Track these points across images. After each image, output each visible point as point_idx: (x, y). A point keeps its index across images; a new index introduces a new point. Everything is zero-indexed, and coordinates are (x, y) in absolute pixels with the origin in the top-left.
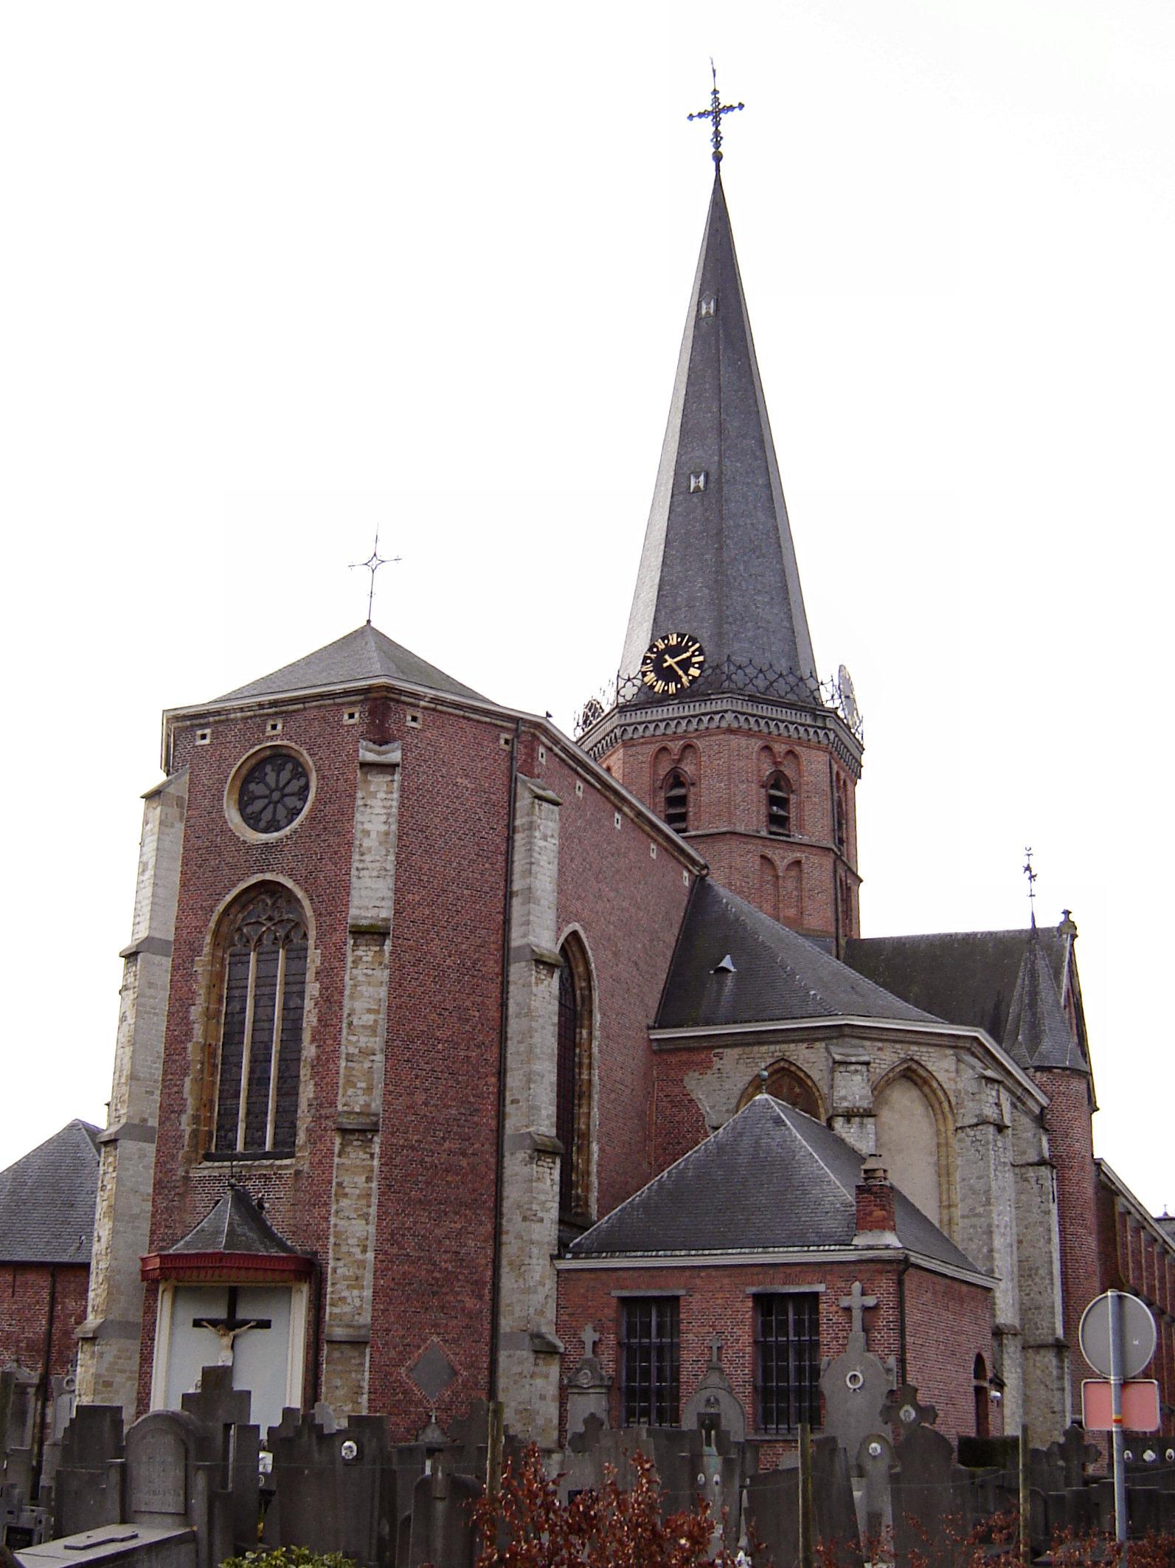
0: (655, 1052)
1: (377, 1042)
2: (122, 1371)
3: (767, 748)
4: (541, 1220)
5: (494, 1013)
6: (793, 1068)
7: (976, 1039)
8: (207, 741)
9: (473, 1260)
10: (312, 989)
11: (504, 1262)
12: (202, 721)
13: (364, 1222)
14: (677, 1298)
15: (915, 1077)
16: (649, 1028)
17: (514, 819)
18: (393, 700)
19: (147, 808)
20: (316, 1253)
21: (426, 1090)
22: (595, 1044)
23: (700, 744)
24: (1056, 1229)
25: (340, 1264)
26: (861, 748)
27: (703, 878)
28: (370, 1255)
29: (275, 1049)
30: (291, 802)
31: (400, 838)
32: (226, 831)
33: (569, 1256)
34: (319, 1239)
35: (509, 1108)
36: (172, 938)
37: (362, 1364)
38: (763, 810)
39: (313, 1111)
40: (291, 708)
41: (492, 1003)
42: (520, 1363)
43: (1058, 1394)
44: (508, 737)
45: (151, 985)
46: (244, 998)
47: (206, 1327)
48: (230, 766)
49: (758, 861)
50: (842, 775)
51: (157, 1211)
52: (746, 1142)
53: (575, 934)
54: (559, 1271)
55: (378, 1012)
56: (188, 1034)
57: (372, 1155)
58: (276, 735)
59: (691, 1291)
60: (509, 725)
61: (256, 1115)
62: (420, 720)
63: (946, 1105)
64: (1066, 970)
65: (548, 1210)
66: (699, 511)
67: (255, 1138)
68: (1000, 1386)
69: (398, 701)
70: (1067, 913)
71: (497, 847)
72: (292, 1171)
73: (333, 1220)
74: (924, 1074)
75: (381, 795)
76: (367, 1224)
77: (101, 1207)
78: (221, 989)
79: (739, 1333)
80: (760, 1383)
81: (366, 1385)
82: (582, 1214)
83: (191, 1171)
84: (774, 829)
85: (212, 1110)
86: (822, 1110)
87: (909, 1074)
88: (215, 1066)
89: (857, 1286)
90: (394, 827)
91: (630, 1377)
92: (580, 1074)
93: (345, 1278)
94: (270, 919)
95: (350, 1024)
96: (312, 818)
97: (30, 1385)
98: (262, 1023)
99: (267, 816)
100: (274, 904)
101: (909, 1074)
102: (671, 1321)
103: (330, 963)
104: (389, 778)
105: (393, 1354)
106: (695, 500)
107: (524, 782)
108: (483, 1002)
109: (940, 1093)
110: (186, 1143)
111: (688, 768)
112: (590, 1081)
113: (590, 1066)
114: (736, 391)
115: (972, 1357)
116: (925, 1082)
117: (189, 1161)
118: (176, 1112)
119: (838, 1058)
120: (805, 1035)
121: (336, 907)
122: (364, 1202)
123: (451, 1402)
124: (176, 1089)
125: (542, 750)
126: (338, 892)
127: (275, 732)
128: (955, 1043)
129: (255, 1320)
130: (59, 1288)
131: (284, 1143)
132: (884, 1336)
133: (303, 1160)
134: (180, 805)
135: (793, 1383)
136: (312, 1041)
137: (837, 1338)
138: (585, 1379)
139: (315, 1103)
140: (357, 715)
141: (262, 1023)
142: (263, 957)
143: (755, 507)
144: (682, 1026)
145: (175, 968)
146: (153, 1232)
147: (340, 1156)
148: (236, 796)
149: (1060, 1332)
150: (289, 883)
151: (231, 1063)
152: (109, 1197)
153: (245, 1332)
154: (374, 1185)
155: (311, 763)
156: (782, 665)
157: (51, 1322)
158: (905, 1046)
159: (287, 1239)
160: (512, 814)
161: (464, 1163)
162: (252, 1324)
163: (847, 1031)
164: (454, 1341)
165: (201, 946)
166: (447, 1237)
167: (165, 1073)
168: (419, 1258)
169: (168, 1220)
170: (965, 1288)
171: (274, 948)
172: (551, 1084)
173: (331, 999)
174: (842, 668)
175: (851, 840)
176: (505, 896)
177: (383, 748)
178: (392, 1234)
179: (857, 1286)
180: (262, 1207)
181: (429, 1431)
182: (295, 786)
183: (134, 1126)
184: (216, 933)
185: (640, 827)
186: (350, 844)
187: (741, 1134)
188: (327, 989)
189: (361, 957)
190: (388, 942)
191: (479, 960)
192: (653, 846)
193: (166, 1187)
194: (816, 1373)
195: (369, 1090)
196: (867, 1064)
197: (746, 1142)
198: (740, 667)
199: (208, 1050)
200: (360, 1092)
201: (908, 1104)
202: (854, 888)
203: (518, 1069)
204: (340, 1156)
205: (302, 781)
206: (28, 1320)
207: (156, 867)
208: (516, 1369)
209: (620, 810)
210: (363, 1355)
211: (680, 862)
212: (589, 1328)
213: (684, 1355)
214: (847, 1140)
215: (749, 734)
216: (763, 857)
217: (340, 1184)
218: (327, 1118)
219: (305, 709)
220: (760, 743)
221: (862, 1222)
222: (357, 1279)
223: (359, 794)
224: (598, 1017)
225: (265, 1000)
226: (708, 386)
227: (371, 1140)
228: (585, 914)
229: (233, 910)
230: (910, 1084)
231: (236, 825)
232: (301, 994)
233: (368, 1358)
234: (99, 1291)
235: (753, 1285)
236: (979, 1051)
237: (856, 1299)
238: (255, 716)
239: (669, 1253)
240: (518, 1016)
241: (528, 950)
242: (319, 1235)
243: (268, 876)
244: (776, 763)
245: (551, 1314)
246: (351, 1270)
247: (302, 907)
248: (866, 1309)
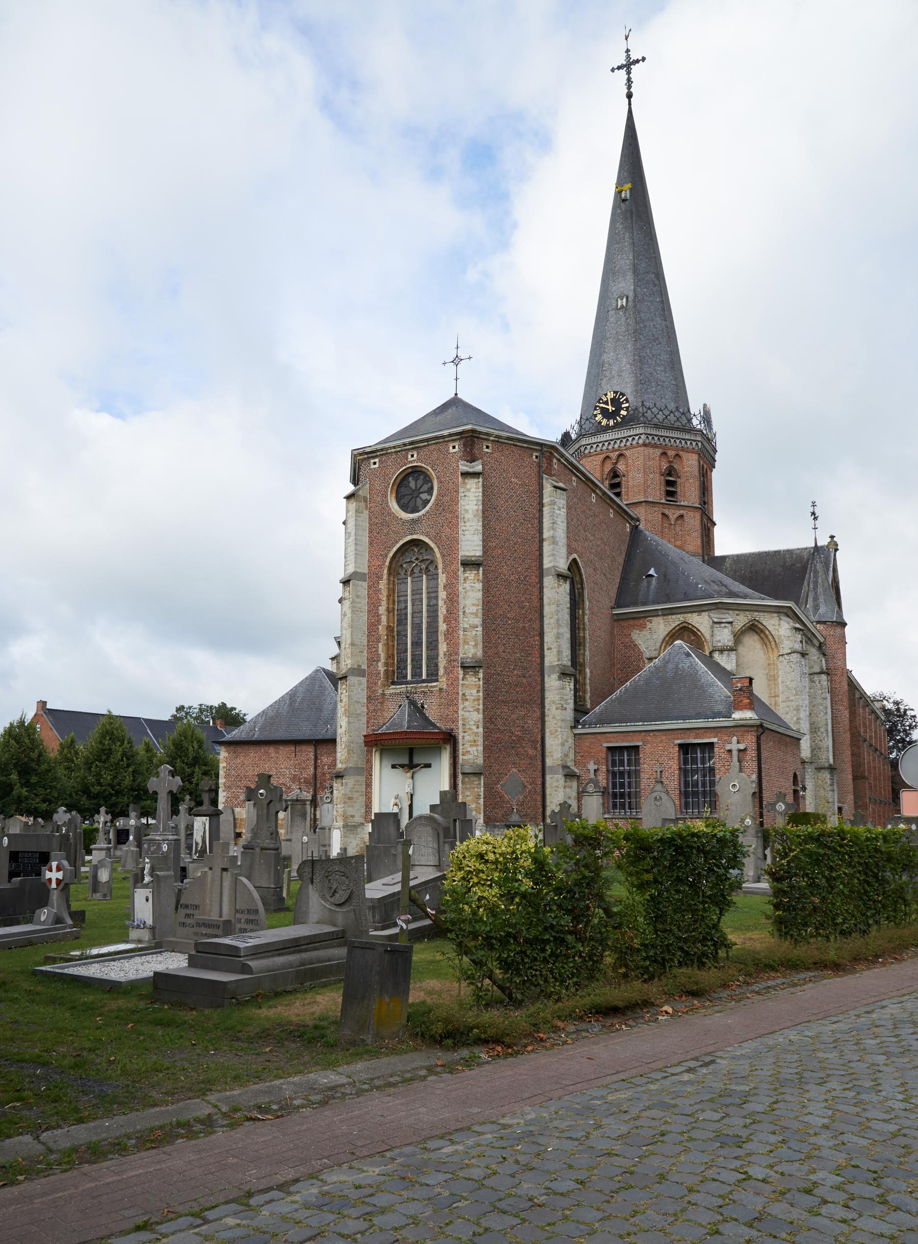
0: (615, 620)
1: (478, 621)
3: (664, 454)
4: (566, 709)
5: (536, 603)
6: (690, 627)
7: (790, 607)
8: (377, 466)
9: (531, 730)
10: (442, 595)
11: (547, 730)
12: (373, 455)
14: (638, 747)
15: (757, 630)
16: (612, 608)
17: (542, 499)
18: (476, 437)
19: (347, 504)
20: (452, 729)
21: (504, 645)
22: (586, 617)
23: (627, 453)
24: (829, 707)
25: (466, 734)
26: (715, 451)
27: (637, 527)
28: (481, 730)
29: (424, 626)
30: (424, 496)
31: (483, 513)
32: (390, 513)
33: (580, 727)
35: (546, 652)
36: (366, 571)
37: (480, 784)
38: (663, 488)
40: (421, 445)
41: (535, 599)
42: (557, 781)
43: (831, 793)
44: (537, 454)
45: (358, 596)
46: (406, 602)
48: (390, 479)
49: (660, 515)
50: (705, 466)
52: (671, 666)
53: (574, 560)
54: (575, 735)
55: (478, 605)
56: (379, 621)
57: (479, 679)
58: (413, 459)
59: (645, 742)
60: (538, 448)
61: (417, 660)
62: (490, 448)
63: (773, 643)
64: (831, 569)
65: (568, 704)
66: (623, 319)
67: (417, 672)
68: (804, 789)
69: (478, 438)
70: (832, 537)
71: (534, 515)
73: (461, 713)
74: (762, 627)
75: (473, 490)
77: (340, 710)
78: (394, 597)
79: (671, 763)
80: (683, 789)
81: (482, 794)
82: (582, 705)
84: (668, 499)
85: (393, 660)
86: (706, 648)
87: (753, 628)
88: (393, 637)
89: (735, 739)
90: (481, 507)
91: (614, 786)
92: (579, 633)
93: (469, 741)
94: (417, 559)
95: (464, 612)
96: (436, 504)
97: (308, 800)
98: (417, 613)
99: (411, 505)
100: (419, 551)
101: (753, 628)
102: (635, 759)
103: (451, 581)
104: (477, 480)
105: (494, 778)
106: (621, 313)
107: (547, 479)
108: (530, 598)
109: (770, 637)
111: (621, 467)
112: (584, 637)
113: (584, 629)
114: (643, 245)
115: (792, 775)
116: (762, 631)
117: (384, 685)
119: (716, 620)
120: (669, 611)
121: (452, 551)
123: (524, 801)
125: (555, 461)
126: (451, 544)
127: (413, 459)
128: (779, 610)
130: (318, 752)
131: (432, 675)
132: (751, 763)
133: (443, 682)
134: (365, 501)
135: (700, 789)
136: (444, 621)
137: (724, 766)
138: (591, 788)
140: (457, 447)
141: (417, 613)
142: (414, 580)
143: (655, 315)
144: (629, 606)
145: (369, 587)
146: (368, 722)
147: (463, 680)
148: (394, 495)
149: (831, 761)
150: (427, 540)
151: (402, 635)
152: (345, 705)
153: (419, 770)
154: (481, 694)
155: (434, 474)
156: (672, 406)
157: (316, 768)
158: (752, 613)
160: (541, 497)
161: (524, 681)
163: (720, 606)
164: (524, 771)
165: (382, 575)
166: (518, 719)
167: (368, 641)
168: (505, 730)
170: (788, 739)
171: (420, 575)
172: (568, 639)
173: (453, 600)
174: (705, 406)
175: (710, 503)
176: (539, 541)
177: (473, 464)
178: (490, 719)
179: (735, 739)
180: (423, 707)
181: (513, 816)
182: (425, 488)
183: (355, 669)
184: (390, 568)
185: (605, 501)
186: (457, 517)
187: (668, 662)
188: (450, 594)
189: (468, 577)
190: (481, 569)
191: (527, 576)
192: (611, 511)
194: (713, 783)
195: (476, 645)
196: (731, 623)
197: (671, 666)
198: (649, 409)
199: (389, 629)
201: (752, 643)
202: (711, 528)
203: (550, 632)
204: (463, 680)
205: (429, 485)
206: (304, 768)
207: (356, 535)
208: (555, 784)
209: (594, 492)
210: (480, 779)
211: (625, 518)
212: (592, 763)
213: (642, 775)
214: (721, 663)
215: (655, 446)
216: (663, 514)
217: (464, 695)
219: (428, 445)
220: (661, 451)
221: (738, 706)
223: (461, 490)
224: (587, 603)
225: (417, 601)
226: (626, 244)
227: (478, 672)
228: (579, 549)
229: (398, 556)
230: (754, 634)
231: (396, 510)
232: (437, 598)
233: (482, 781)
234: (343, 753)
235: (678, 739)
236: (791, 614)
237: (734, 746)
238: (402, 450)
239: (633, 724)
240: (549, 604)
241: (553, 570)
243: (415, 537)
244: (669, 462)
245: (572, 756)
247: (434, 552)
248: (740, 751)
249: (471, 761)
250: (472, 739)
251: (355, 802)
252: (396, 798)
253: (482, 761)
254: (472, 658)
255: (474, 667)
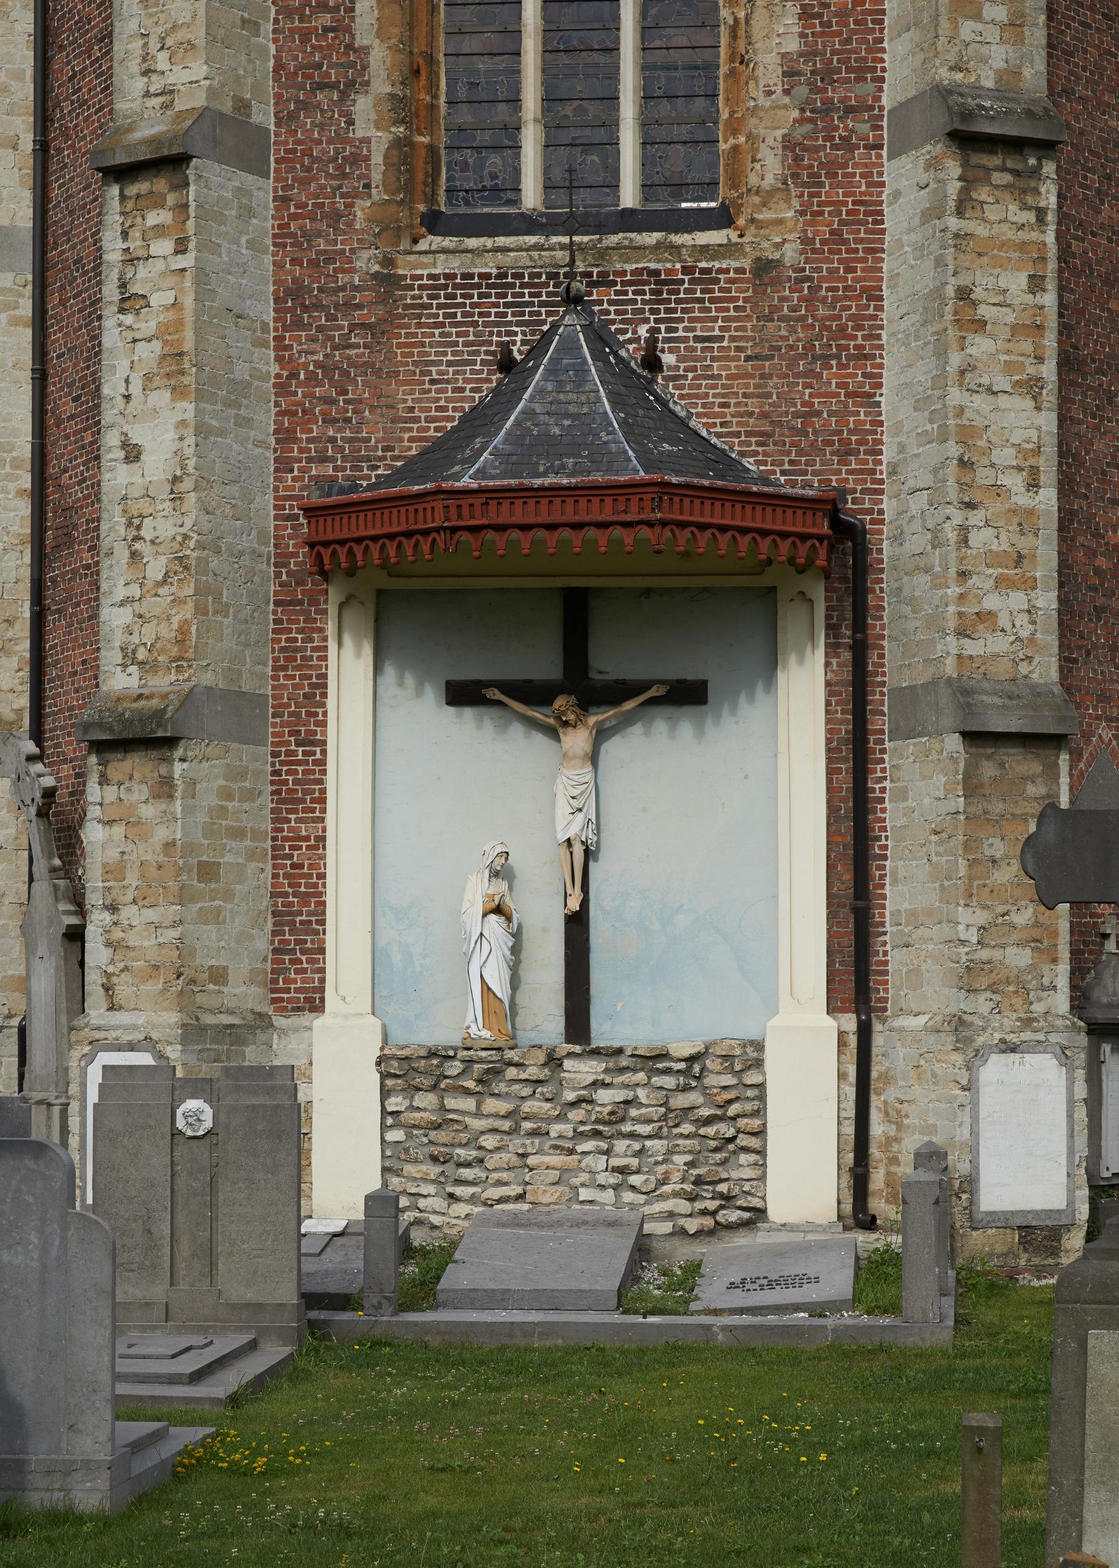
2: (238, 833)
13: (1031, 403)
25: (976, 518)
34: (846, 452)
39: (802, 91)
47: (499, 703)
51: (293, 375)
57: (1041, 213)
72: (746, 263)
76: (1038, 409)
83: (401, 259)
93: (993, 559)
110: (377, 176)
118: (334, 86)
122: (1027, 346)
124: (326, 19)
129: (662, 682)
139: (807, 68)
146: (286, 437)
147: (960, 212)
154: (1049, 299)
159: (742, 454)
162: (654, 692)
169: (334, 402)
180: (652, 363)
193: (318, 306)
200: (992, 34)
218: (849, 110)
222: (1020, 558)
227: (1036, 173)
233: (1064, 780)
242: (845, 442)
246: (1003, 537)
249: (1002, 670)
250: (1002, 545)
251: (228, 895)
252: (495, 874)
253: (1054, 674)
254: (998, 93)
255: (1016, 145)
